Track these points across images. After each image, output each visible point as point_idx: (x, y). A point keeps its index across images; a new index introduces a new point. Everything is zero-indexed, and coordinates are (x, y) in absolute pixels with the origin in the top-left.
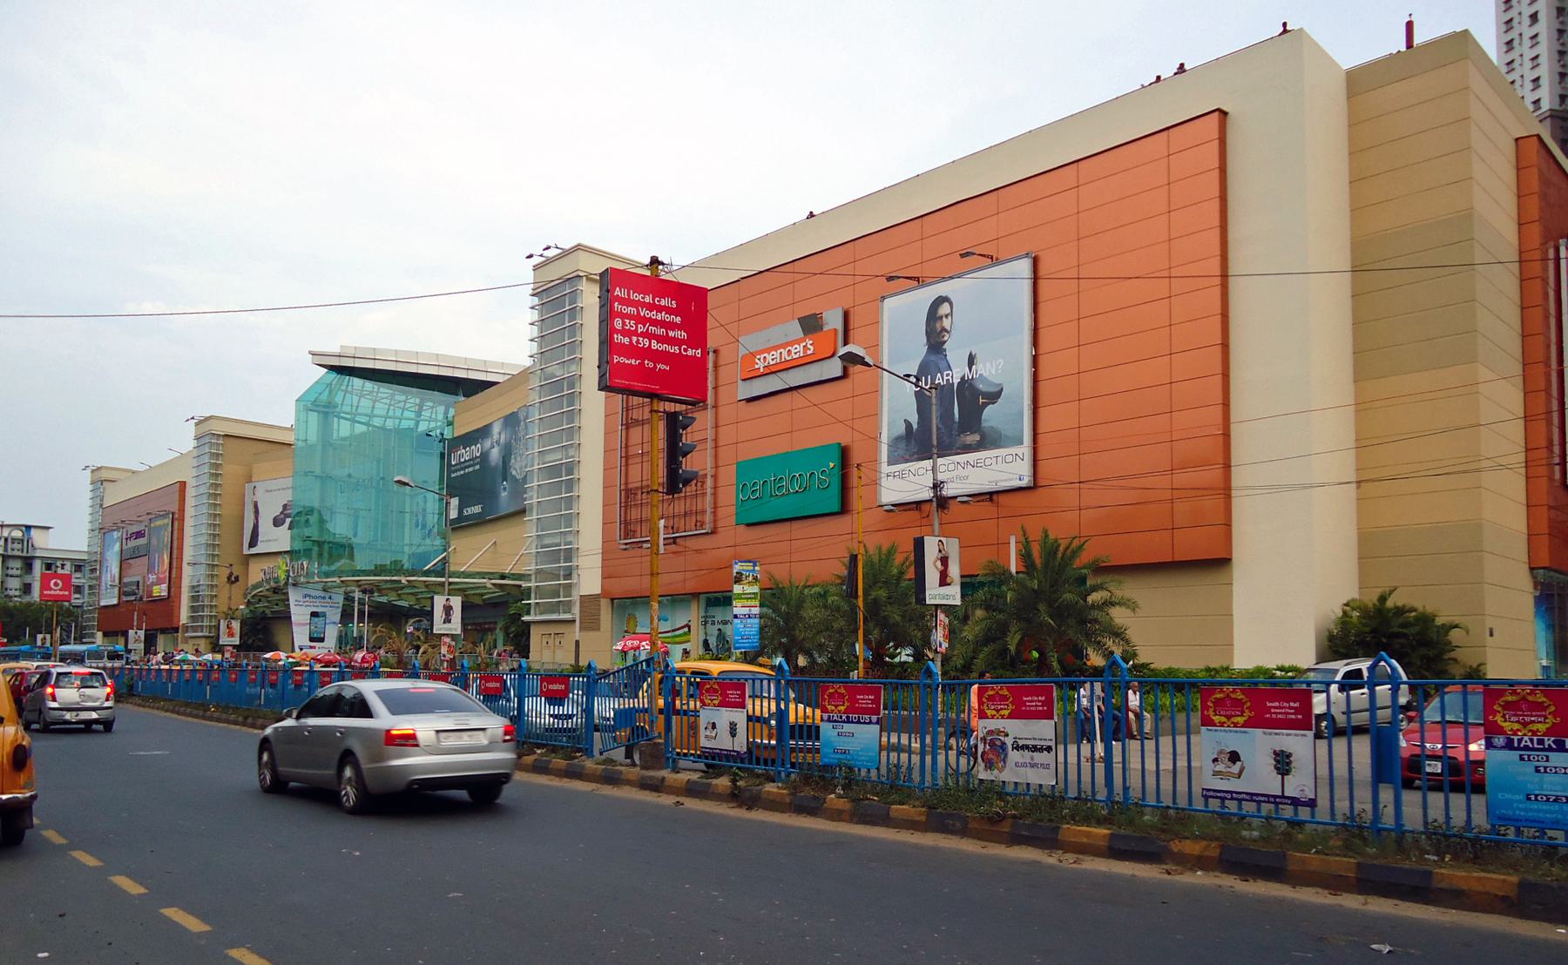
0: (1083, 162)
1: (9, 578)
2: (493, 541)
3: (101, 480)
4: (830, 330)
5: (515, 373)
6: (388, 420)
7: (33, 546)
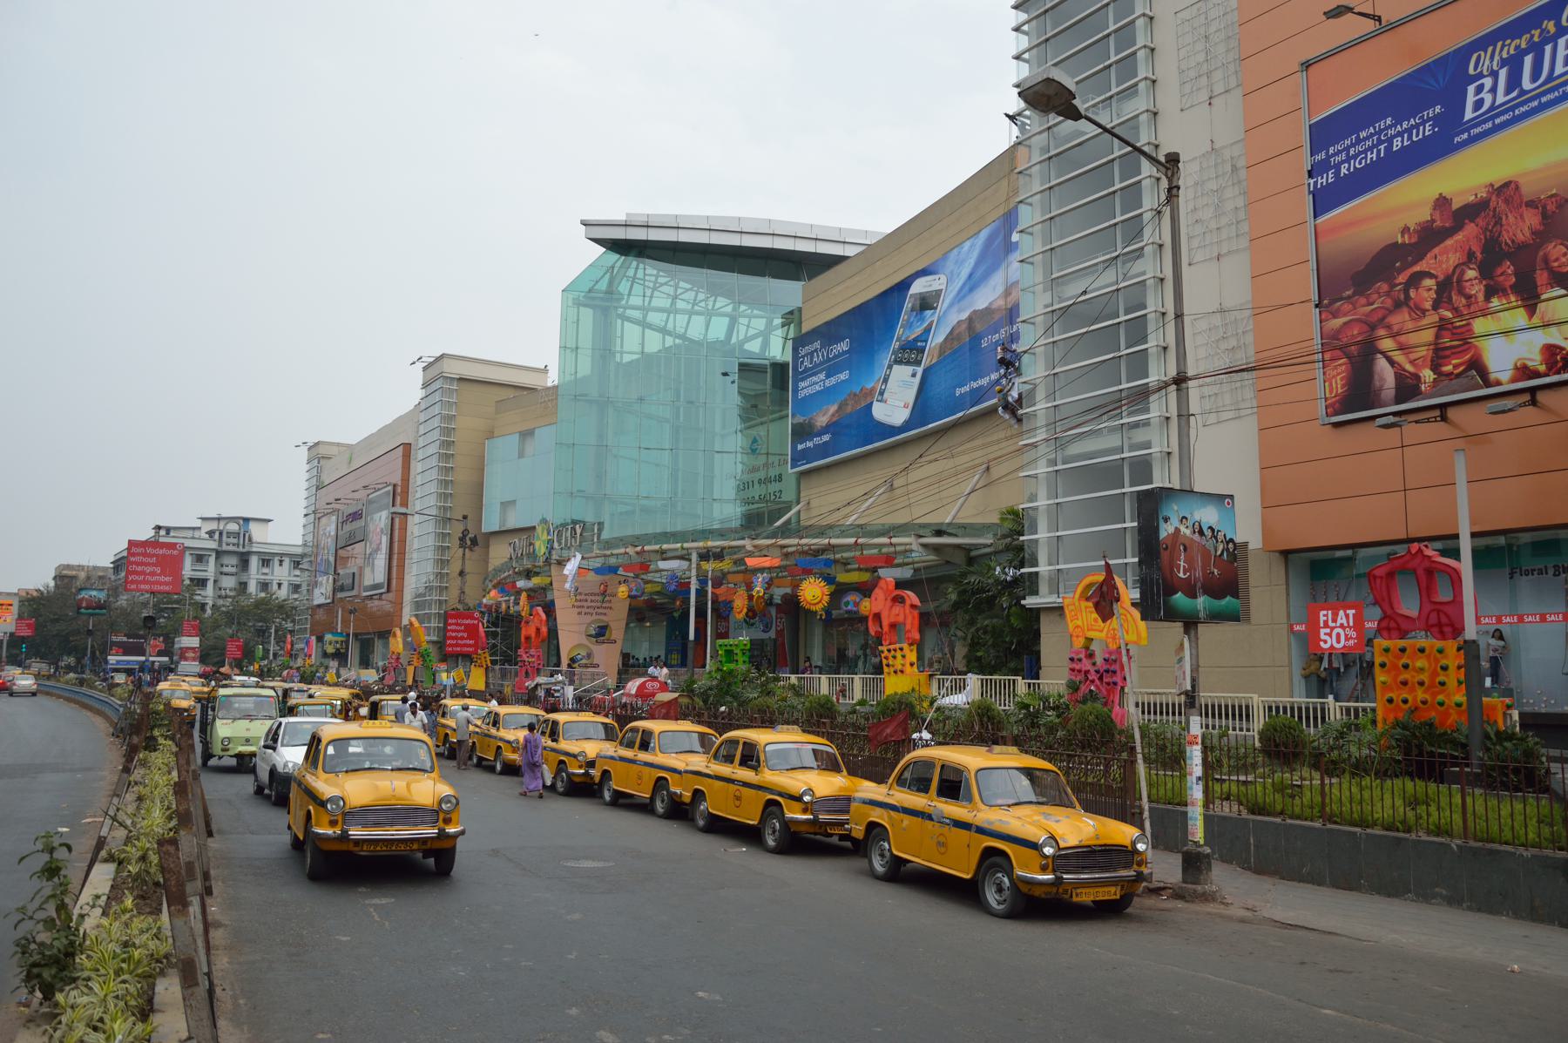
1: (224, 577)
3: (318, 454)
4: (289, 789)
7: (250, 540)
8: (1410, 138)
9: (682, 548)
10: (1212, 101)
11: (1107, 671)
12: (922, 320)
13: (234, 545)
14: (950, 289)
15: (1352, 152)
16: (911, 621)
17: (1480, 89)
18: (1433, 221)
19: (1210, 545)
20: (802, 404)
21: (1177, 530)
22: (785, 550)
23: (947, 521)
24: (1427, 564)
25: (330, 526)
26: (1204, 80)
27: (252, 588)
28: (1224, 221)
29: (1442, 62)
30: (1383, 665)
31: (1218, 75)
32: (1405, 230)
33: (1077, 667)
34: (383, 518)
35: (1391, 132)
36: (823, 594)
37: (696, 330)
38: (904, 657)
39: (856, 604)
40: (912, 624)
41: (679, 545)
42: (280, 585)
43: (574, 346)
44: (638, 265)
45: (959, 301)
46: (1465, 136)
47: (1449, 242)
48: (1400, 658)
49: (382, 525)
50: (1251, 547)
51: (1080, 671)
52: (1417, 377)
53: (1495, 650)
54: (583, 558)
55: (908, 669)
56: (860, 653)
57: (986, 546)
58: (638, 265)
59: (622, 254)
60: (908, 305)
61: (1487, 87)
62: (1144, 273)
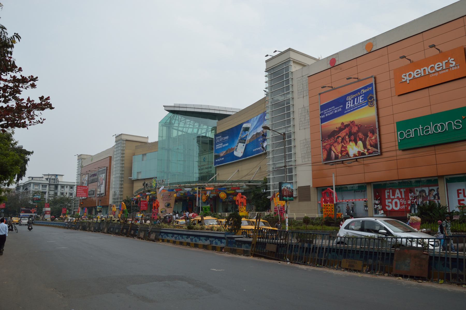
0: (424, 33)
1: (50, 191)
2: (238, 170)
3: (81, 158)
5: (238, 111)
6: (189, 129)
7: (58, 181)
8: (337, 111)
9: (190, 185)
10: (304, 97)
11: (281, 210)
12: (246, 133)
13: (53, 182)
14: (252, 127)
15: (328, 112)
16: (244, 201)
17: (348, 103)
18: (341, 127)
19: (289, 190)
20: (217, 151)
21: (284, 188)
22: (214, 186)
23: (251, 180)
24: (330, 191)
25: (86, 177)
26: (302, 92)
27: (59, 194)
28: (306, 121)
29: (343, 97)
30: (324, 208)
31: (305, 92)
32: (337, 128)
33: (276, 210)
34: (103, 176)
35: (334, 109)
36: (225, 196)
37: (190, 131)
38: (243, 209)
40: (245, 202)
41: (189, 185)
42: (66, 193)
43: (162, 136)
44: (177, 116)
45: (254, 130)
46: (346, 112)
47: (344, 131)
48: (326, 207)
49: (103, 178)
50: (311, 186)
51: (276, 210)
52: (338, 155)
53: (353, 206)
54: (165, 187)
55: (244, 211)
56: (231, 209)
57: (260, 185)
58: (177, 116)
59: (173, 113)
60: (242, 129)
61: (350, 103)
62: (291, 131)
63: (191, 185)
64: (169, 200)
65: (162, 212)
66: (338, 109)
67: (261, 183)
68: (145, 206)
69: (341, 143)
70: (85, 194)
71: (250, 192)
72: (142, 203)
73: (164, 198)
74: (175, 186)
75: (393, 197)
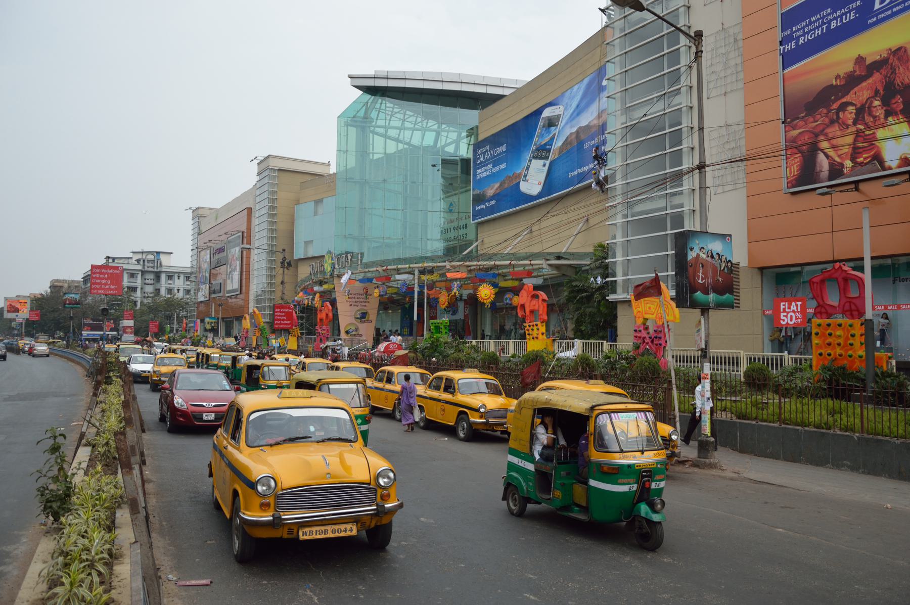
3: (198, 215)
7: (161, 264)
8: (841, 21)
9: (410, 267)
11: (656, 337)
12: (549, 132)
13: (152, 267)
14: (565, 114)
15: (806, 30)
16: (542, 308)
18: (855, 71)
19: (717, 264)
20: (479, 183)
21: (698, 255)
22: (469, 268)
25: (206, 256)
27: (163, 292)
28: (729, 72)
30: (817, 334)
32: (838, 77)
33: (639, 335)
34: (237, 251)
35: (830, 17)
36: (491, 294)
37: (416, 139)
38: (538, 329)
39: (511, 300)
40: (543, 311)
41: (407, 266)
42: (178, 290)
45: (571, 121)
46: (875, 19)
47: (864, 84)
50: (741, 265)
51: (640, 337)
53: (883, 325)
54: (352, 273)
55: (540, 336)
56: (513, 327)
59: (372, 95)
60: (541, 124)
63: (411, 266)
64: (365, 304)
65: (347, 332)
66: (843, 14)
67: (589, 259)
68: (285, 318)
69: (855, 123)
70: (115, 287)
71: (561, 285)
72: (279, 310)
73: (352, 300)
74: (375, 269)
75: (789, 310)
